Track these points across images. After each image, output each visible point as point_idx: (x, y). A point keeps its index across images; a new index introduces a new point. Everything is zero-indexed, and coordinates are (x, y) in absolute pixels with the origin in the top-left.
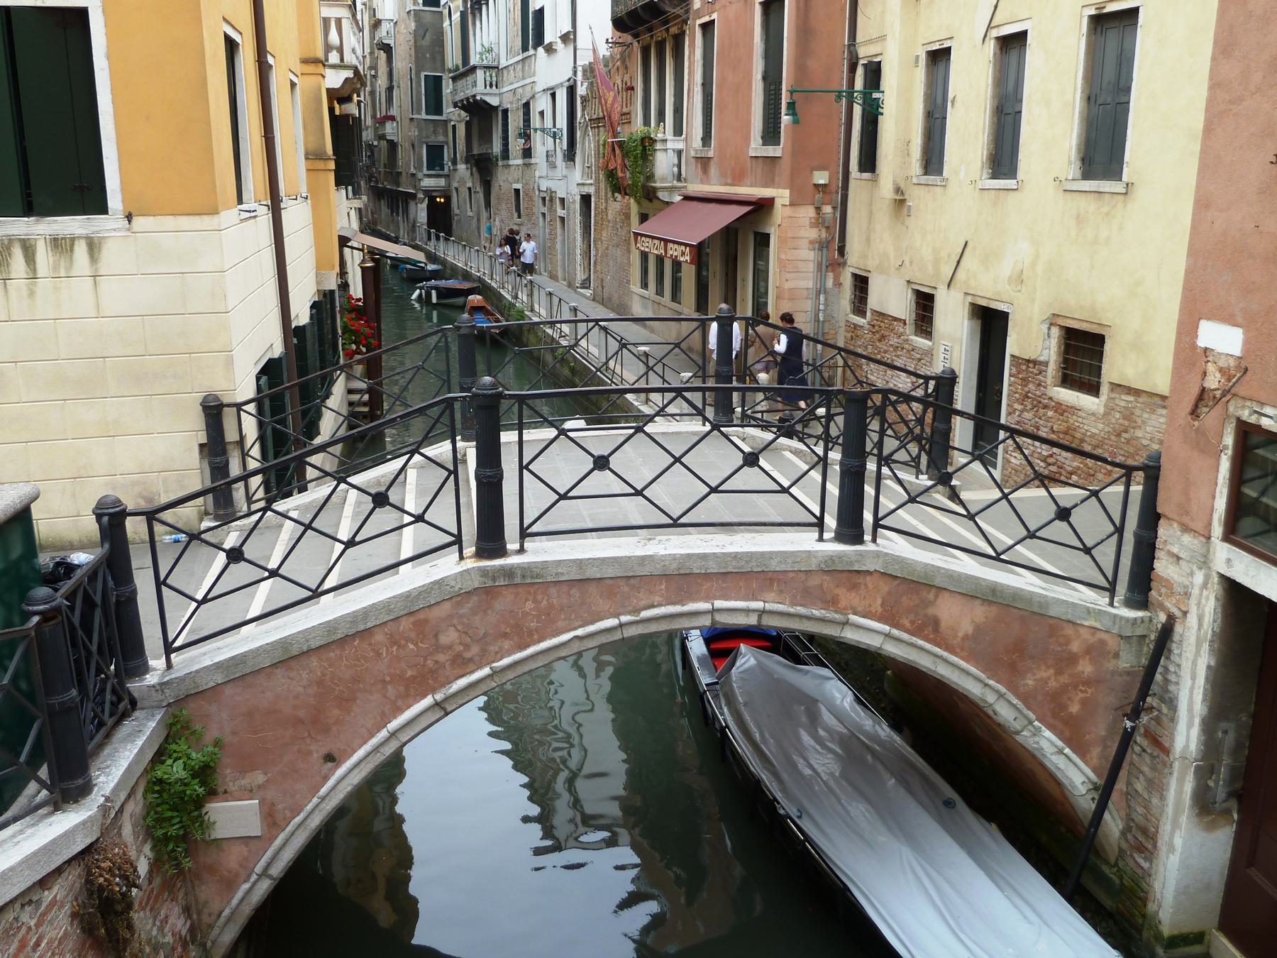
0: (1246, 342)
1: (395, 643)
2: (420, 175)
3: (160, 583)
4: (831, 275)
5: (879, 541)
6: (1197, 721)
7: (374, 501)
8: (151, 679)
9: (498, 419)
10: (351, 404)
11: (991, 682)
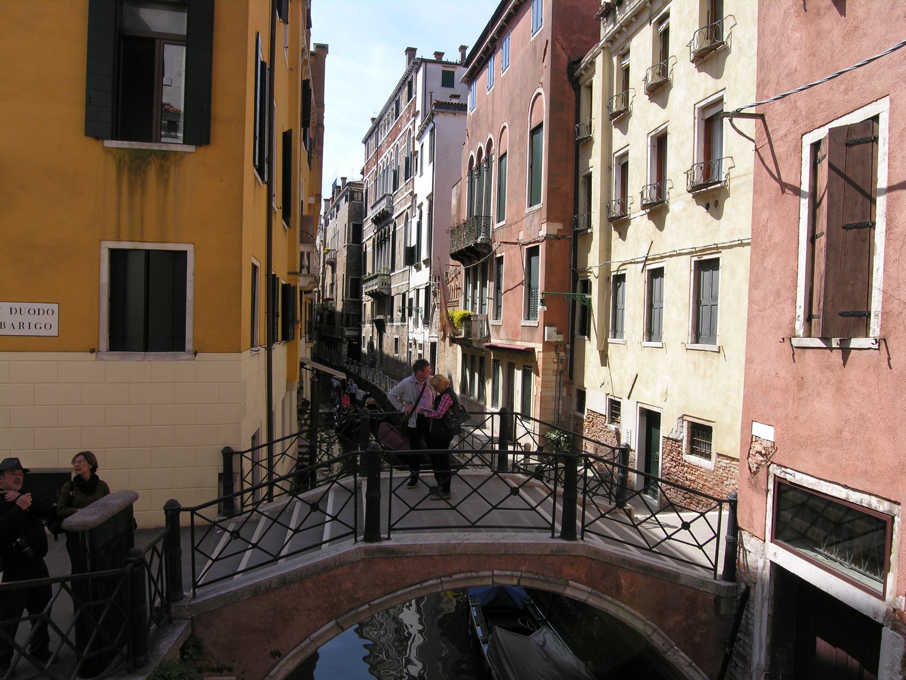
0: (775, 434)
3: (194, 549)
4: (565, 389)
5: (585, 539)
6: (764, 646)
8: (184, 602)
9: (379, 391)
10: (299, 453)
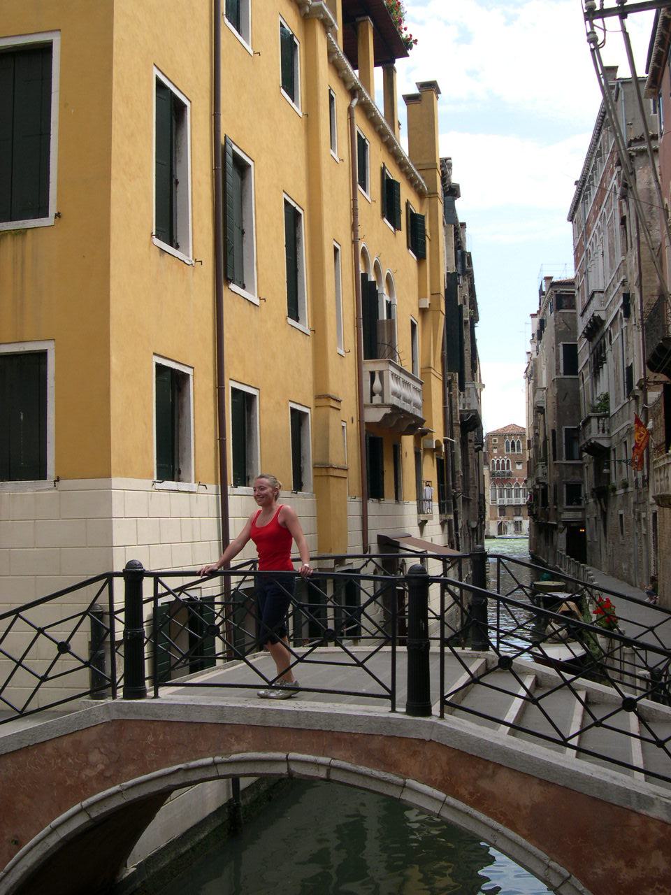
1: (60, 756)
2: (560, 510)
7: (59, 648)
11: (553, 864)
